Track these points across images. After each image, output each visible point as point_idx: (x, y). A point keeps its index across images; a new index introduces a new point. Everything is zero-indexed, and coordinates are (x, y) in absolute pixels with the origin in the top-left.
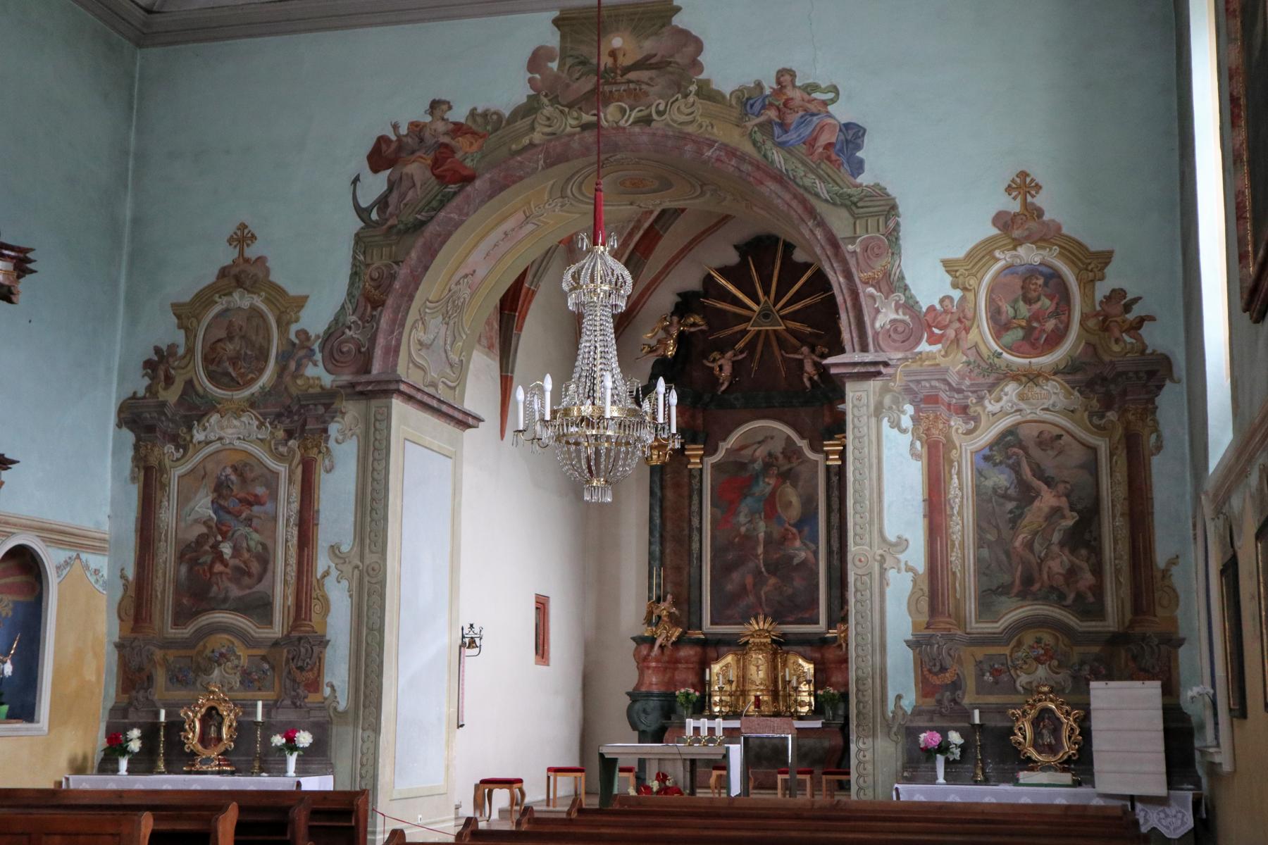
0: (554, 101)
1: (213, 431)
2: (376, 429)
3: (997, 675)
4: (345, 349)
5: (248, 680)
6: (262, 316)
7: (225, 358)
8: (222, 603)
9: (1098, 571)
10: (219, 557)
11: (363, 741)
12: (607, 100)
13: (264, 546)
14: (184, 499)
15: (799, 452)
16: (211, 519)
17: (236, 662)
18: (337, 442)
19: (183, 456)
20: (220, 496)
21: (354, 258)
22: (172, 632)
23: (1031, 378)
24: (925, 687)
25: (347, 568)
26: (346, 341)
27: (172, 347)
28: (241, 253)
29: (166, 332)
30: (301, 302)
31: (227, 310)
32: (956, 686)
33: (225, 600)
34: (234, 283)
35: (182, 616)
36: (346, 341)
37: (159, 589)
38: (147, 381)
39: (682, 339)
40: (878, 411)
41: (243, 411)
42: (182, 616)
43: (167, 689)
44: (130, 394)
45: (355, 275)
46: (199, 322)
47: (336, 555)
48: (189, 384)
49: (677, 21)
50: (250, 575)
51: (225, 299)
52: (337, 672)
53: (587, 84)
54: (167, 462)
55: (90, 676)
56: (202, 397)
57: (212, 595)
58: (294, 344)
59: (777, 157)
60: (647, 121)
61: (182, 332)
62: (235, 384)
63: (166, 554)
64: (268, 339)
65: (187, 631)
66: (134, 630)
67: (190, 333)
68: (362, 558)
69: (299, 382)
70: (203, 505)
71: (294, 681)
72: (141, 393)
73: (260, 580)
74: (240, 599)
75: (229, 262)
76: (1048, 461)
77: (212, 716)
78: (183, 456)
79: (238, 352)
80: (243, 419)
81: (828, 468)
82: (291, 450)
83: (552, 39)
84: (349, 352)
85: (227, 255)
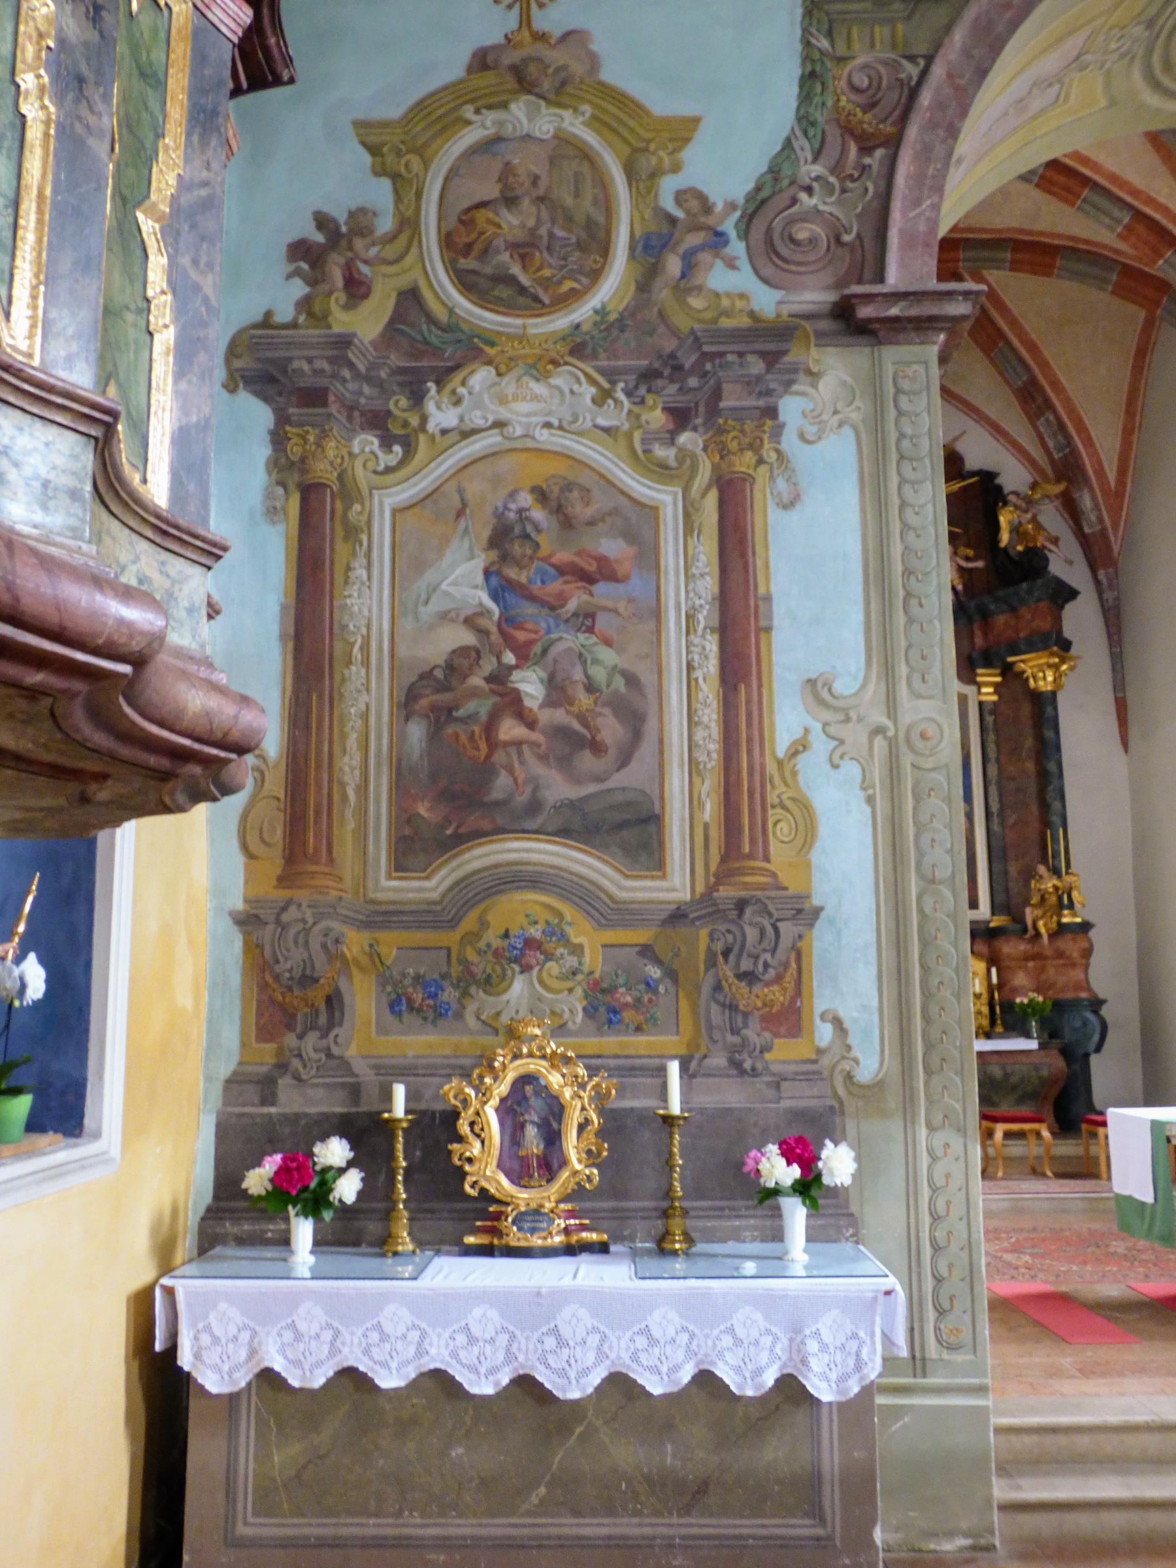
1: (479, 405)
2: (900, 413)
4: (802, 235)
5: (604, 1008)
6: (585, 155)
7: (499, 243)
8: (525, 817)
10: (513, 703)
11: (933, 1158)
13: (632, 680)
14: (409, 565)
16: (484, 612)
17: (571, 961)
18: (802, 437)
19: (402, 463)
20: (505, 557)
21: (807, 44)
22: (391, 887)
25: (856, 735)
26: (804, 218)
27: (361, 222)
28: (526, 20)
29: (346, 183)
30: (682, 131)
31: (498, 139)
33: (534, 807)
34: (510, 83)
35: (414, 847)
36: (804, 218)
37: (351, 780)
38: (299, 289)
41: (555, 363)
42: (414, 847)
43: (382, 1030)
44: (257, 315)
45: (811, 79)
46: (426, 164)
47: (821, 702)
48: (410, 298)
50: (597, 748)
51: (491, 117)
54: (361, 476)
55: (184, 998)
56: (446, 329)
57: (496, 794)
58: (673, 221)
61: (386, 184)
62: (527, 301)
63: (367, 697)
64: (607, 204)
65: (432, 885)
66: (284, 880)
67: (404, 186)
68: (891, 706)
69: (696, 302)
70: (462, 577)
71: (733, 1007)
72: (285, 313)
73: (625, 760)
74: (572, 805)
75: (494, 37)
78: (402, 463)
79: (533, 232)
80: (556, 381)
81: (981, 704)
82: (684, 455)
84: (813, 241)
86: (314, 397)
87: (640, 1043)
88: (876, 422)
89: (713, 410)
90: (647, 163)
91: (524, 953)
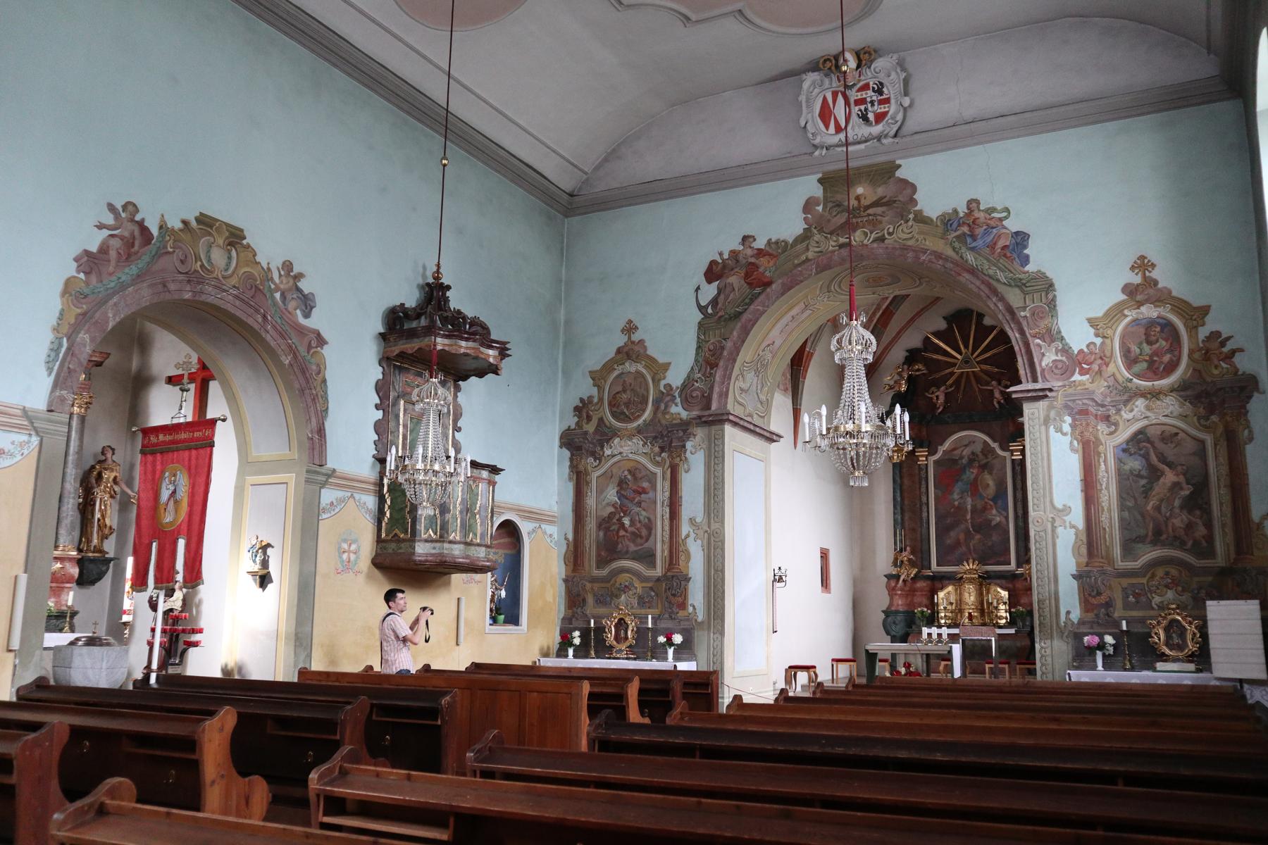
0: (821, 231)
3: (1139, 597)
5: (642, 602)
9: (1209, 525)
12: (854, 228)
13: (649, 519)
14: (600, 491)
15: (993, 450)
22: (596, 572)
23: (1154, 395)
24: (1086, 604)
25: (701, 532)
28: (629, 338)
30: (666, 366)
32: (1109, 605)
33: (627, 552)
35: (601, 563)
38: (576, 419)
39: (910, 380)
40: (1047, 422)
42: (601, 563)
45: (699, 348)
49: (900, 174)
50: (641, 537)
52: (696, 597)
53: (842, 218)
59: (970, 257)
60: (882, 239)
63: (591, 525)
65: (604, 572)
67: (600, 388)
72: (573, 426)
74: (636, 552)
76: (1169, 451)
77: (621, 624)
83: (818, 192)
85: (621, 340)
86: (1084, 412)
87: (643, 611)
88: (709, 448)
89: (670, 446)
90: (657, 377)
91: (626, 589)
